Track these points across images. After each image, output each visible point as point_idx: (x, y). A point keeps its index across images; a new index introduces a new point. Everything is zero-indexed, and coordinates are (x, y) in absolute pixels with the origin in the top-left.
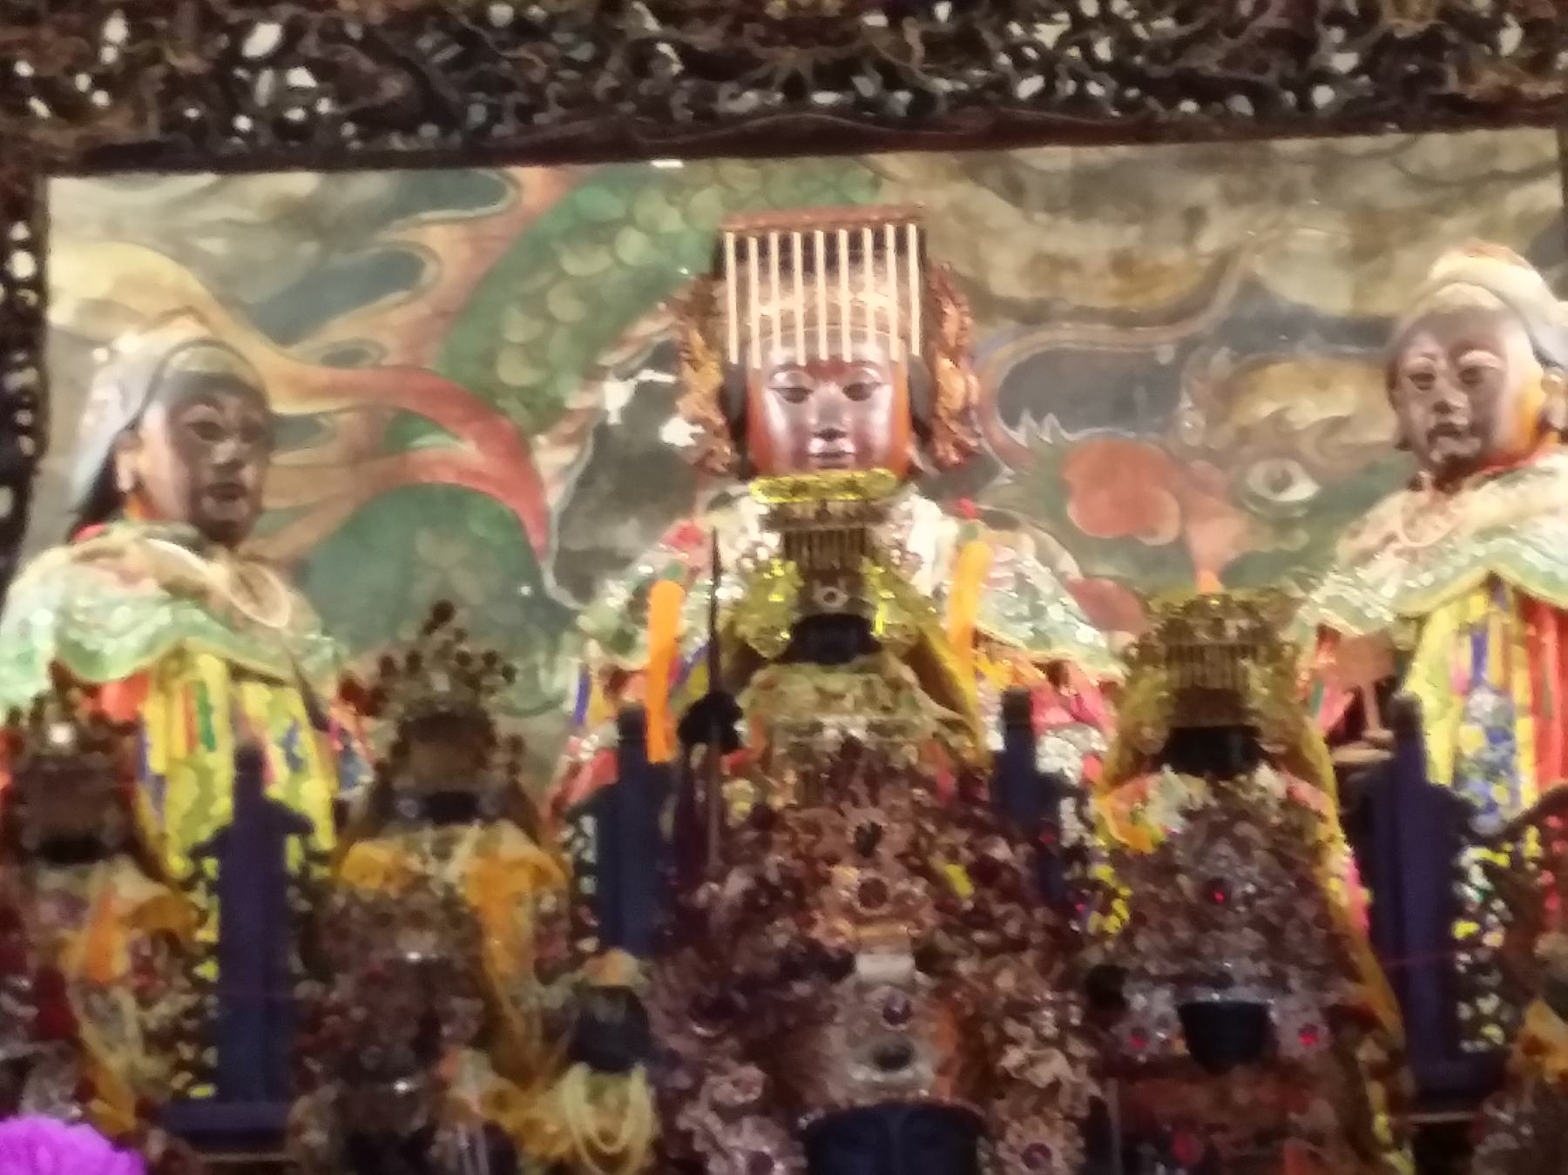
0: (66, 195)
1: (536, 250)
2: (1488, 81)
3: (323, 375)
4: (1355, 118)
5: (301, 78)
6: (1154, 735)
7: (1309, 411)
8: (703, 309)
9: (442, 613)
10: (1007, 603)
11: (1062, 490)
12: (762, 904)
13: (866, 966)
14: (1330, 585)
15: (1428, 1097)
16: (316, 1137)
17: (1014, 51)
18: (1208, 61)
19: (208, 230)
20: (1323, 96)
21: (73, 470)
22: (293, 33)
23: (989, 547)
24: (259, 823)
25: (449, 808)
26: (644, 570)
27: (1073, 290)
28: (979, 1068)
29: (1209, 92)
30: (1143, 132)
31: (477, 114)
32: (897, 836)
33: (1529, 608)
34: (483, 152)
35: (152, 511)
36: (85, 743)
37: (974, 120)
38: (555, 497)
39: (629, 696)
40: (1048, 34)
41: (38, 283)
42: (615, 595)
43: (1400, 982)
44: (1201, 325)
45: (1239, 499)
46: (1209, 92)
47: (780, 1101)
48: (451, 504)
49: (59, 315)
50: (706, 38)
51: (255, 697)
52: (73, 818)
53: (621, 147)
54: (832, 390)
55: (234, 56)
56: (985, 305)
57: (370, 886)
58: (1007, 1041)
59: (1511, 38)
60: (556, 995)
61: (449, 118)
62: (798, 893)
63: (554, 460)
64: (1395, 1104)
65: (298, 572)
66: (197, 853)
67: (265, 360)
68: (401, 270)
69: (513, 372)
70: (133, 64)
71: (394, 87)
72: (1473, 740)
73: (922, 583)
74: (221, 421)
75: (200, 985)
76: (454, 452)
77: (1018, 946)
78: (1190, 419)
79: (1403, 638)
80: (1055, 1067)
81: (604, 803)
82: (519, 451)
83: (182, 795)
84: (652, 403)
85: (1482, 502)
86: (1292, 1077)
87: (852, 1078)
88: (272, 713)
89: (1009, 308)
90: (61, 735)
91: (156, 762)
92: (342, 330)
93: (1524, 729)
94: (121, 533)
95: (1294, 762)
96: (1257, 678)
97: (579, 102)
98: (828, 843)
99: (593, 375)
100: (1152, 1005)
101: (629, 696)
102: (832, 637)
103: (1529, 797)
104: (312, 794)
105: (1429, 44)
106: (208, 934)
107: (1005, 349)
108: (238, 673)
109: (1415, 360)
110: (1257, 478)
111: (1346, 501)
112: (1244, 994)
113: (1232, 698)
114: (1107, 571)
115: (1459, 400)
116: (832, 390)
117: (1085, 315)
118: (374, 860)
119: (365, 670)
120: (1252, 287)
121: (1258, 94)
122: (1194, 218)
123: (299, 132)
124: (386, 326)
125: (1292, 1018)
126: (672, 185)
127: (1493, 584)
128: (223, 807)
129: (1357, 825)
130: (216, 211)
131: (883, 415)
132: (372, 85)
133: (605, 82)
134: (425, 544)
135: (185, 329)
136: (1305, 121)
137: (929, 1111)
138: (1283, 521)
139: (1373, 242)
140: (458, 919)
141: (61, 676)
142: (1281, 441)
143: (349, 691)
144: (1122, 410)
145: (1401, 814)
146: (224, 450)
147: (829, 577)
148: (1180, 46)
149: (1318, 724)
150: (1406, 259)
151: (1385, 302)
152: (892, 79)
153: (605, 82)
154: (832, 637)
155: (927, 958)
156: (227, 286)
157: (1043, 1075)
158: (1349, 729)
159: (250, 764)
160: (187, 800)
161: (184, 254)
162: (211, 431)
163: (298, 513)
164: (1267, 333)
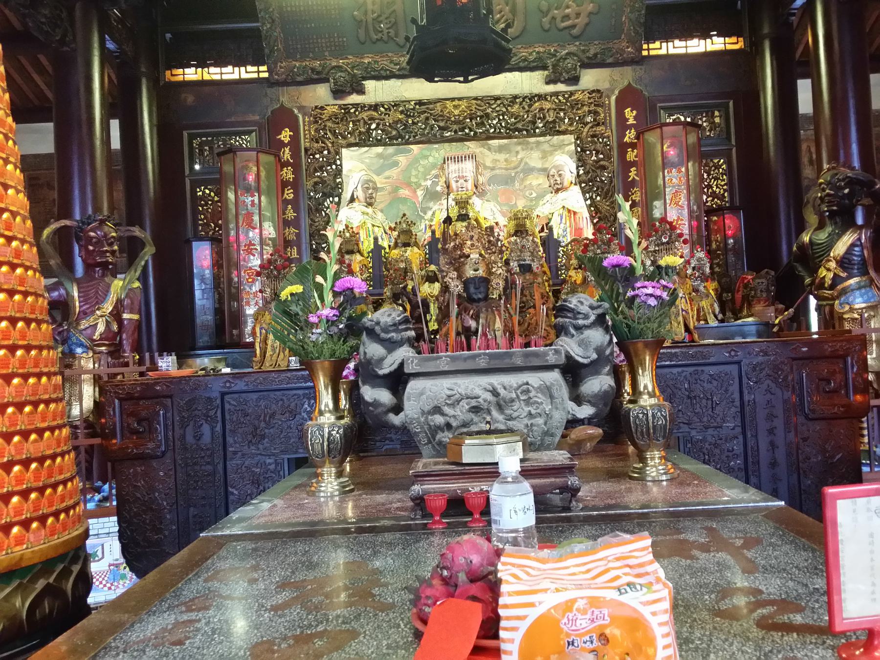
0: (344, 151)
1: (416, 161)
2: (563, 127)
3: (385, 181)
4: (542, 134)
5: (380, 132)
6: (512, 232)
7: (535, 183)
8: (443, 169)
9: (404, 215)
10: (489, 212)
11: (498, 196)
12: (455, 248)
13: (472, 256)
14: (539, 208)
15: (554, 285)
16: (388, 294)
17: (490, 125)
18: (520, 126)
19: (366, 158)
20: (537, 131)
21: (346, 196)
22: (378, 125)
23: (486, 204)
24: (378, 248)
25: (406, 245)
26: (434, 209)
27: (499, 165)
28: (490, 273)
29: (520, 131)
30: (510, 137)
31: (407, 137)
32: (476, 237)
33: (569, 211)
34: (408, 143)
35: (360, 201)
36: (351, 236)
37: (484, 136)
38: (420, 199)
39: (433, 228)
40: (495, 122)
41: (341, 165)
42: (430, 213)
43: (550, 268)
44: (518, 170)
45: (525, 197)
46: (520, 131)
47: (459, 277)
48: (404, 200)
49: (344, 172)
50: (442, 124)
51: (376, 229)
52: (350, 248)
53: (429, 142)
54: (462, 181)
55: (369, 128)
56: (486, 167)
57: (395, 257)
58: (493, 267)
59: (566, 121)
60: (423, 272)
61: (403, 138)
62: (461, 246)
63: (420, 193)
64: (549, 286)
65: (382, 211)
66: (368, 253)
67: (376, 178)
68: (396, 164)
69: (413, 180)
70: (354, 130)
71: (394, 133)
72: (561, 232)
73: (477, 209)
74: (370, 188)
75: (370, 273)
76: (404, 192)
77: (494, 253)
78: (517, 184)
79: (550, 216)
80: (500, 271)
81: (429, 244)
82: (415, 192)
83: (366, 244)
84: (435, 184)
85: (561, 195)
86: (536, 275)
87: (470, 273)
88: (379, 232)
89: (489, 168)
90: (348, 235)
91: (362, 239)
92: (387, 173)
93: (568, 230)
94: (355, 204)
95: (533, 235)
96: (528, 222)
97: (423, 135)
98: (466, 238)
99: (426, 180)
100: (514, 265)
101: (433, 228)
102: (463, 217)
103: (569, 240)
104: (385, 244)
105: (554, 122)
106: (371, 265)
107: (488, 174)
108: (373, 226)
109: (551, 173)
110: (527, 194)
111: (541, 196)
112: (527, 262)
113: (524, 225)
114: (505, 208)
115: (558, 179)
116: (462, 181)
117: (502, 168)
118: (395, 253)
119: (393, 226)
120: (526, 163)
121: (527, 131)
122: (517, 152)
123: (380, 140)
124: (394, 172)
125: (535, 266)
126: (437, 149)
127: (564, 207)
128: (372, 247)
129: (543, 245)
130: (367, 155)
131: (470, 185)
132: (391, 133)
133: (427, 131)
134: (401, 206)
135: (364, 173)
136: (535, 135)
137: (481, 278)
138: (531, 200)
139: (544, 156)
140: (407, 261)
141: (347, 226)
142: (531, 187)
143: (390, 228)
144: (506, 183)
145: (550, 243)
146: (370, 191)
147: (463, 208)
148: (515, 123)
149: (537, 230)
150: (550, 158)
151: (546, 166)
152: (471, 130)
153: (427, 131)
154: (463, 217)
155: (481, 255)
156: (369, 167)
157: (498, 272)
158: (542, 230)
159: (376, 239)
160: (367, 245)
161: (362, 162)
162: (368, 188)
163: (381, 202)
164: (529, 171)
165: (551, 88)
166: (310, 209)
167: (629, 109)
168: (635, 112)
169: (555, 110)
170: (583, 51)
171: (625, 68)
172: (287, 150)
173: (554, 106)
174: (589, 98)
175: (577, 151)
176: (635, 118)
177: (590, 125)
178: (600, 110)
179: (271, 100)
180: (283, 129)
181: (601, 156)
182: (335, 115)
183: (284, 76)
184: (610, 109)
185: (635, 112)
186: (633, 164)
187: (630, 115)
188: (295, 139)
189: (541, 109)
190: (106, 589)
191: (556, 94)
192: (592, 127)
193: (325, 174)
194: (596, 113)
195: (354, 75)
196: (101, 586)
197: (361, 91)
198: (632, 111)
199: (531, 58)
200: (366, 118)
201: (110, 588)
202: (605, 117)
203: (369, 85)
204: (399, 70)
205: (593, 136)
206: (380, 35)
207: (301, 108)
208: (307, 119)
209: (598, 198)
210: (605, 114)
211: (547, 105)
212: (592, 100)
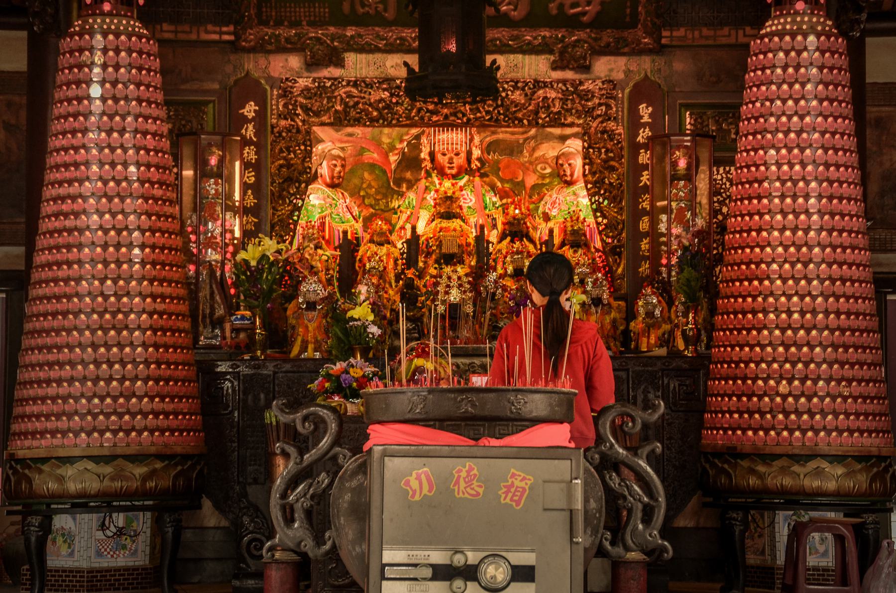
3: (346, 138)
105: (559, 113)
142: (543, 160)
148: (515, 112)
165: (557, 75)
166: (273, 194)
167: (644, 105)
168: (650, 109)
169: (561, 99)
170: (596, 39)
171: (643, 57)
172: (251, 127)
173: (560, 95)
174: (600, 89)
175: (584, 147)
176: (650, 115)
177: (600, 119)
178: (612, 103)
179: (235, 67)
180: (248, 102)
181: (611, 155)
182: (307, 89)
183: (252, 43)
184: (623, 102)
185: (650, 109)
186: (645, 167)
187: (645, 112)
188: (261, 115)
189: (545, 98)
190: (109, 556)
191: (564, 82)
192: (602, 122)
193: (292, 155)
194: (608, 107)
195: (335, 48)
196: (106, 553)
197: (340, 64)
198: (647, 107)
199: (536, 42)
200: (344, 96)
201: (112, 556)
202: (617, 111)
203: (351, 58)
204: (385, 45)
205: (603, 132)
206: (367, 9)
207: (270, 79)
208: (275, 93)
209: (606, 202)
210: (617, 108)
211: (552, 94)
212: (604, 92)
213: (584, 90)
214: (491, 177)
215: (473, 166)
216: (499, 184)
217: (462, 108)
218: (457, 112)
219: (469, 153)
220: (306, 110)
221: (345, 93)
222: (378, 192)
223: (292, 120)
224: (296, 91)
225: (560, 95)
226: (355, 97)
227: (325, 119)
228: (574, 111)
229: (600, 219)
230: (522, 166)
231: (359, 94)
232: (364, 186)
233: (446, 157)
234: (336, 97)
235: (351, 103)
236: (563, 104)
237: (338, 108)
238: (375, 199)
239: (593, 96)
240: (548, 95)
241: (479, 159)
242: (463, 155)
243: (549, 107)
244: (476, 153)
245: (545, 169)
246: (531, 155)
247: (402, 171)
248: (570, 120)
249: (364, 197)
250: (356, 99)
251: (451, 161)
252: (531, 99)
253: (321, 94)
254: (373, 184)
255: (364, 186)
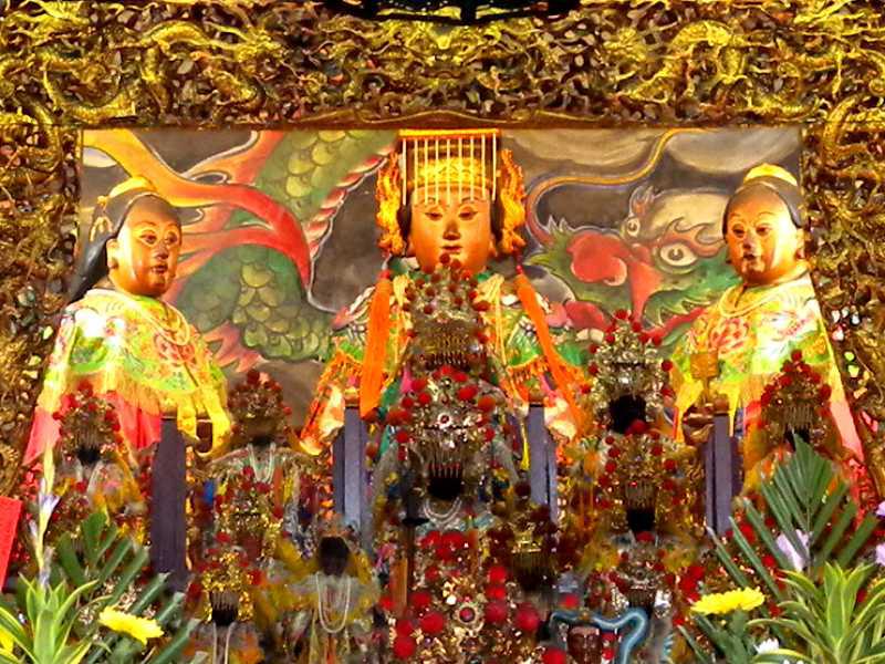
148: (622, 85)
169: (744, 50)
182: (70, 30)
189: (703, 47)
192: (854, 110)
200: (165, 46)
213: (805, 26)
214: (550, 276)
215: (506, 243)
216: (570, 294)
217: (481, 76)
218: (466, 89)
219: (497, 211)
220: (65, 82)
221: (168, 39)
222: (276, 316)
223: (28, 111)
224: (39, 36)
225: (741, 40)
226: (194, 49)
227: (117, 107)
228: (778, 84)
229: (854, 371)
230: (624, 250)
231: (205, 42)
232: (245, 300)
233: (440, 225)
234: (143, 50)
235: (185, 69)
236: (750, 61)
237: (150, 76)
238: (271, 333)
239: (827, 42)
240: (710, 40)
241: (519, 229)
242: (483, 217)
243: (711, 70)
244: (514, 211)
245: (681, 255)
246: (645, 224)
247: (334, 263)
248: (767, 105)
249: (241, 329)
250: (197, 55)
251: (451, 233)
252: (663, 50)
253: (105, 43)
254: (265, 294)
255: (245, 300)
